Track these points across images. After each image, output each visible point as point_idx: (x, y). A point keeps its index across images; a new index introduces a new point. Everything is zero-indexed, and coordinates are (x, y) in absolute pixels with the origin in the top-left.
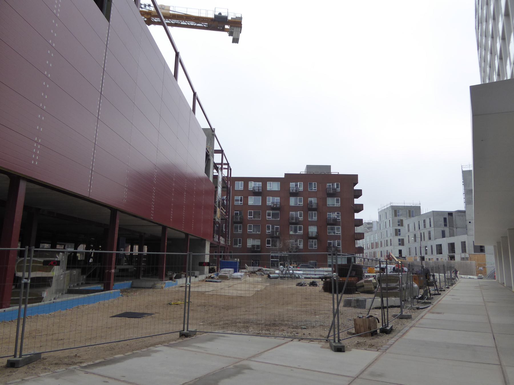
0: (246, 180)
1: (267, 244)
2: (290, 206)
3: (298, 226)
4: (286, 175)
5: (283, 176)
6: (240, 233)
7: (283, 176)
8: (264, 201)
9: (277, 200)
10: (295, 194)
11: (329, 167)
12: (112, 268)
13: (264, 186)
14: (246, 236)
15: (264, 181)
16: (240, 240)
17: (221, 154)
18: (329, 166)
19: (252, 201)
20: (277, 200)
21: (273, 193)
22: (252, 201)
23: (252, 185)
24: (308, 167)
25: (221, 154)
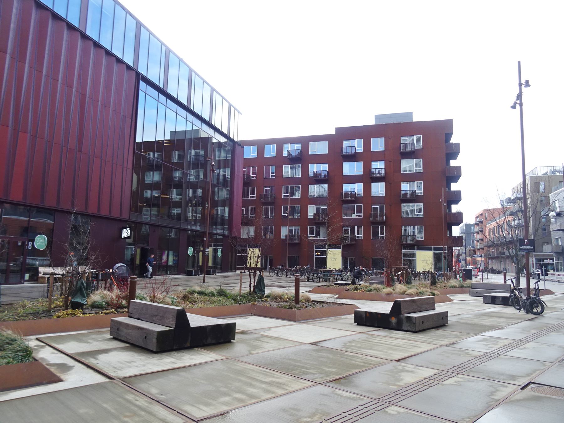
0: (261, 145)
1: (309, 234)
2: (469, 293)
3: (355, 205)
4: (337, 129)
5: (333, 132)
6: (271, 218)
7: (333, 132)
8: (305, 171)
9: (324, 168)
10: (353, 157)
11: (410, 115)
12: (222, 183)
13: (306, 148)
14: (279, 223)
15: (305, 141)
16: (271, 228)
17: (453, 227)
18: (376, 119)
19: (287, 171)
20: (324, 168)
21: (319, 159)
22: (287, 171)
23: (287, 148)
24: (377, 117)
25: (453, 227)
